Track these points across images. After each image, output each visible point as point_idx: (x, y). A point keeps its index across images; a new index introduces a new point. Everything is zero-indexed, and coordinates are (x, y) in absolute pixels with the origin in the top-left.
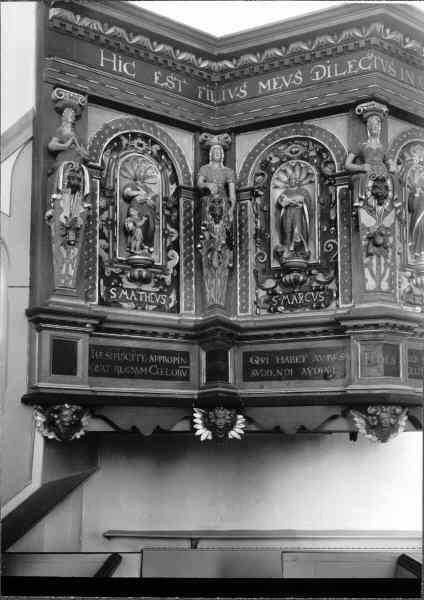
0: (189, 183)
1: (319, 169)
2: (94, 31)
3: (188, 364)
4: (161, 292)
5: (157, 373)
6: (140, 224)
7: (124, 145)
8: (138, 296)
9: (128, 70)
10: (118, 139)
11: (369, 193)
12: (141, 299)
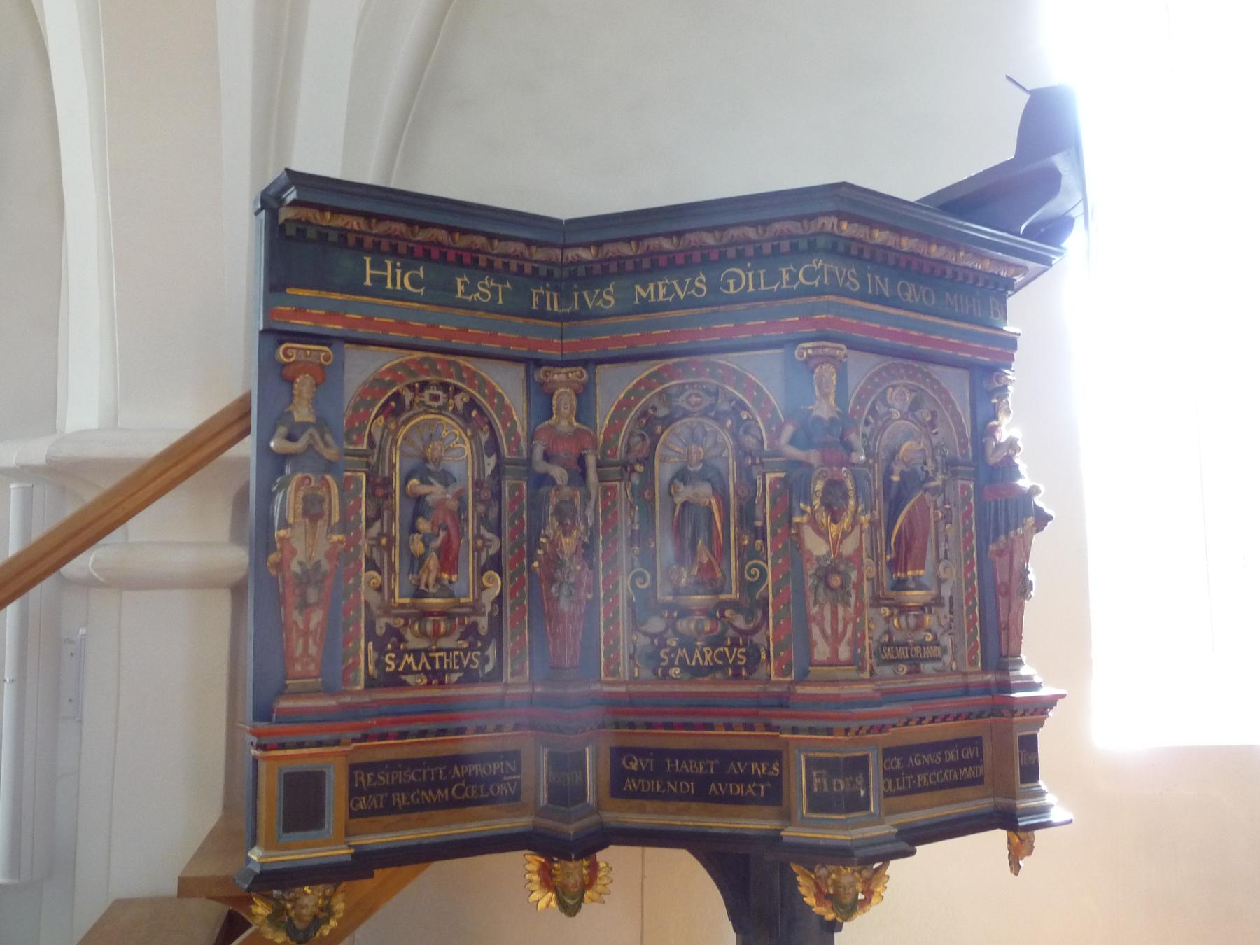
0: (519, 452)
1: (735, 437)
2: (355, 232)
3: (518, 772)
4: (472, 647)
5: (466, 794)
6: (437, 543)
7: (407, 402)
8: (432, 661)
9: (413, 284)
10: (397, 396)
11: (817, 502)
12: (437, 666)
